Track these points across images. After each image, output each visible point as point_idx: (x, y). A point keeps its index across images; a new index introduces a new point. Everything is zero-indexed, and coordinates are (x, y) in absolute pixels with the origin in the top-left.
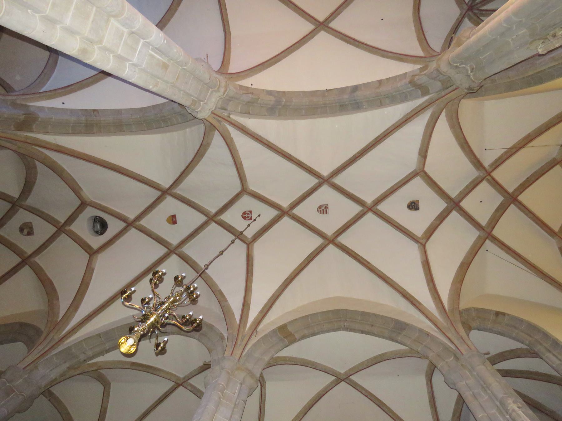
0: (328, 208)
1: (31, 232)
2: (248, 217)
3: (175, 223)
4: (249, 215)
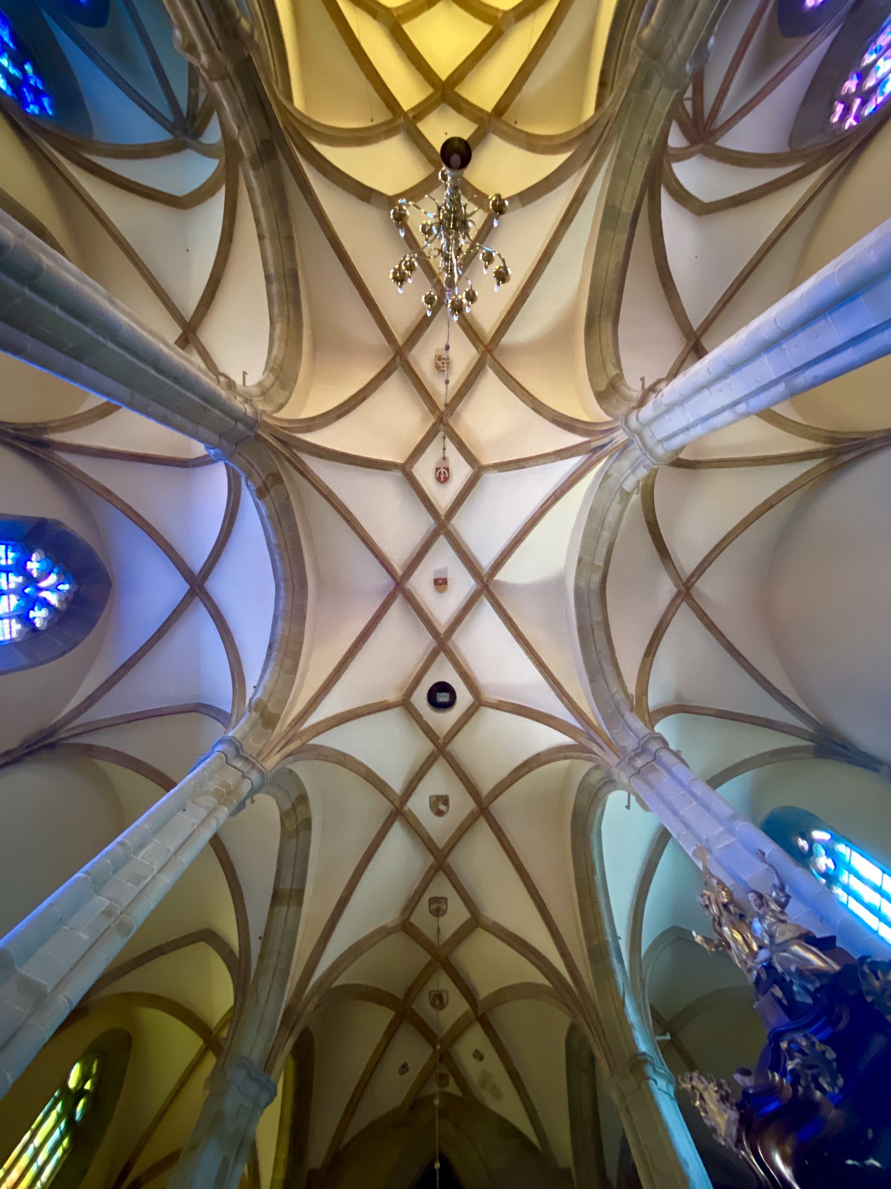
0: (440, 356)
1: (444, 799)
2: (444, 473)
3: (445, 581)
4: (442, 472)
